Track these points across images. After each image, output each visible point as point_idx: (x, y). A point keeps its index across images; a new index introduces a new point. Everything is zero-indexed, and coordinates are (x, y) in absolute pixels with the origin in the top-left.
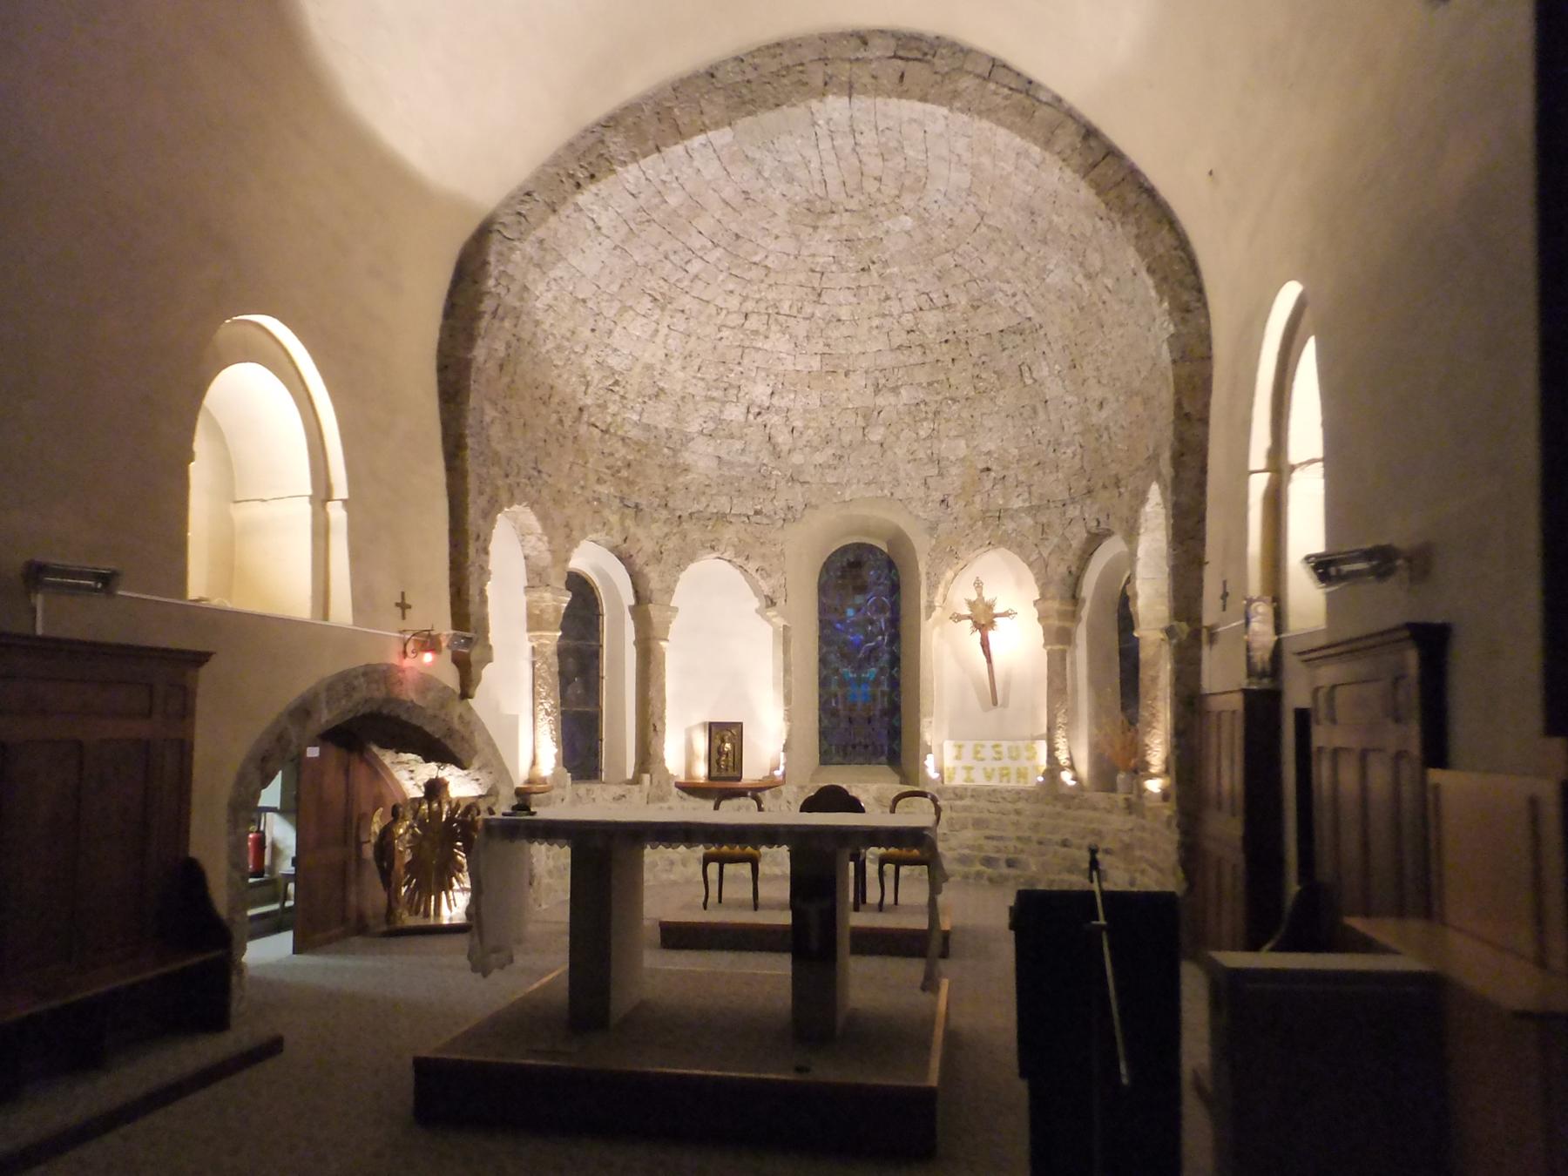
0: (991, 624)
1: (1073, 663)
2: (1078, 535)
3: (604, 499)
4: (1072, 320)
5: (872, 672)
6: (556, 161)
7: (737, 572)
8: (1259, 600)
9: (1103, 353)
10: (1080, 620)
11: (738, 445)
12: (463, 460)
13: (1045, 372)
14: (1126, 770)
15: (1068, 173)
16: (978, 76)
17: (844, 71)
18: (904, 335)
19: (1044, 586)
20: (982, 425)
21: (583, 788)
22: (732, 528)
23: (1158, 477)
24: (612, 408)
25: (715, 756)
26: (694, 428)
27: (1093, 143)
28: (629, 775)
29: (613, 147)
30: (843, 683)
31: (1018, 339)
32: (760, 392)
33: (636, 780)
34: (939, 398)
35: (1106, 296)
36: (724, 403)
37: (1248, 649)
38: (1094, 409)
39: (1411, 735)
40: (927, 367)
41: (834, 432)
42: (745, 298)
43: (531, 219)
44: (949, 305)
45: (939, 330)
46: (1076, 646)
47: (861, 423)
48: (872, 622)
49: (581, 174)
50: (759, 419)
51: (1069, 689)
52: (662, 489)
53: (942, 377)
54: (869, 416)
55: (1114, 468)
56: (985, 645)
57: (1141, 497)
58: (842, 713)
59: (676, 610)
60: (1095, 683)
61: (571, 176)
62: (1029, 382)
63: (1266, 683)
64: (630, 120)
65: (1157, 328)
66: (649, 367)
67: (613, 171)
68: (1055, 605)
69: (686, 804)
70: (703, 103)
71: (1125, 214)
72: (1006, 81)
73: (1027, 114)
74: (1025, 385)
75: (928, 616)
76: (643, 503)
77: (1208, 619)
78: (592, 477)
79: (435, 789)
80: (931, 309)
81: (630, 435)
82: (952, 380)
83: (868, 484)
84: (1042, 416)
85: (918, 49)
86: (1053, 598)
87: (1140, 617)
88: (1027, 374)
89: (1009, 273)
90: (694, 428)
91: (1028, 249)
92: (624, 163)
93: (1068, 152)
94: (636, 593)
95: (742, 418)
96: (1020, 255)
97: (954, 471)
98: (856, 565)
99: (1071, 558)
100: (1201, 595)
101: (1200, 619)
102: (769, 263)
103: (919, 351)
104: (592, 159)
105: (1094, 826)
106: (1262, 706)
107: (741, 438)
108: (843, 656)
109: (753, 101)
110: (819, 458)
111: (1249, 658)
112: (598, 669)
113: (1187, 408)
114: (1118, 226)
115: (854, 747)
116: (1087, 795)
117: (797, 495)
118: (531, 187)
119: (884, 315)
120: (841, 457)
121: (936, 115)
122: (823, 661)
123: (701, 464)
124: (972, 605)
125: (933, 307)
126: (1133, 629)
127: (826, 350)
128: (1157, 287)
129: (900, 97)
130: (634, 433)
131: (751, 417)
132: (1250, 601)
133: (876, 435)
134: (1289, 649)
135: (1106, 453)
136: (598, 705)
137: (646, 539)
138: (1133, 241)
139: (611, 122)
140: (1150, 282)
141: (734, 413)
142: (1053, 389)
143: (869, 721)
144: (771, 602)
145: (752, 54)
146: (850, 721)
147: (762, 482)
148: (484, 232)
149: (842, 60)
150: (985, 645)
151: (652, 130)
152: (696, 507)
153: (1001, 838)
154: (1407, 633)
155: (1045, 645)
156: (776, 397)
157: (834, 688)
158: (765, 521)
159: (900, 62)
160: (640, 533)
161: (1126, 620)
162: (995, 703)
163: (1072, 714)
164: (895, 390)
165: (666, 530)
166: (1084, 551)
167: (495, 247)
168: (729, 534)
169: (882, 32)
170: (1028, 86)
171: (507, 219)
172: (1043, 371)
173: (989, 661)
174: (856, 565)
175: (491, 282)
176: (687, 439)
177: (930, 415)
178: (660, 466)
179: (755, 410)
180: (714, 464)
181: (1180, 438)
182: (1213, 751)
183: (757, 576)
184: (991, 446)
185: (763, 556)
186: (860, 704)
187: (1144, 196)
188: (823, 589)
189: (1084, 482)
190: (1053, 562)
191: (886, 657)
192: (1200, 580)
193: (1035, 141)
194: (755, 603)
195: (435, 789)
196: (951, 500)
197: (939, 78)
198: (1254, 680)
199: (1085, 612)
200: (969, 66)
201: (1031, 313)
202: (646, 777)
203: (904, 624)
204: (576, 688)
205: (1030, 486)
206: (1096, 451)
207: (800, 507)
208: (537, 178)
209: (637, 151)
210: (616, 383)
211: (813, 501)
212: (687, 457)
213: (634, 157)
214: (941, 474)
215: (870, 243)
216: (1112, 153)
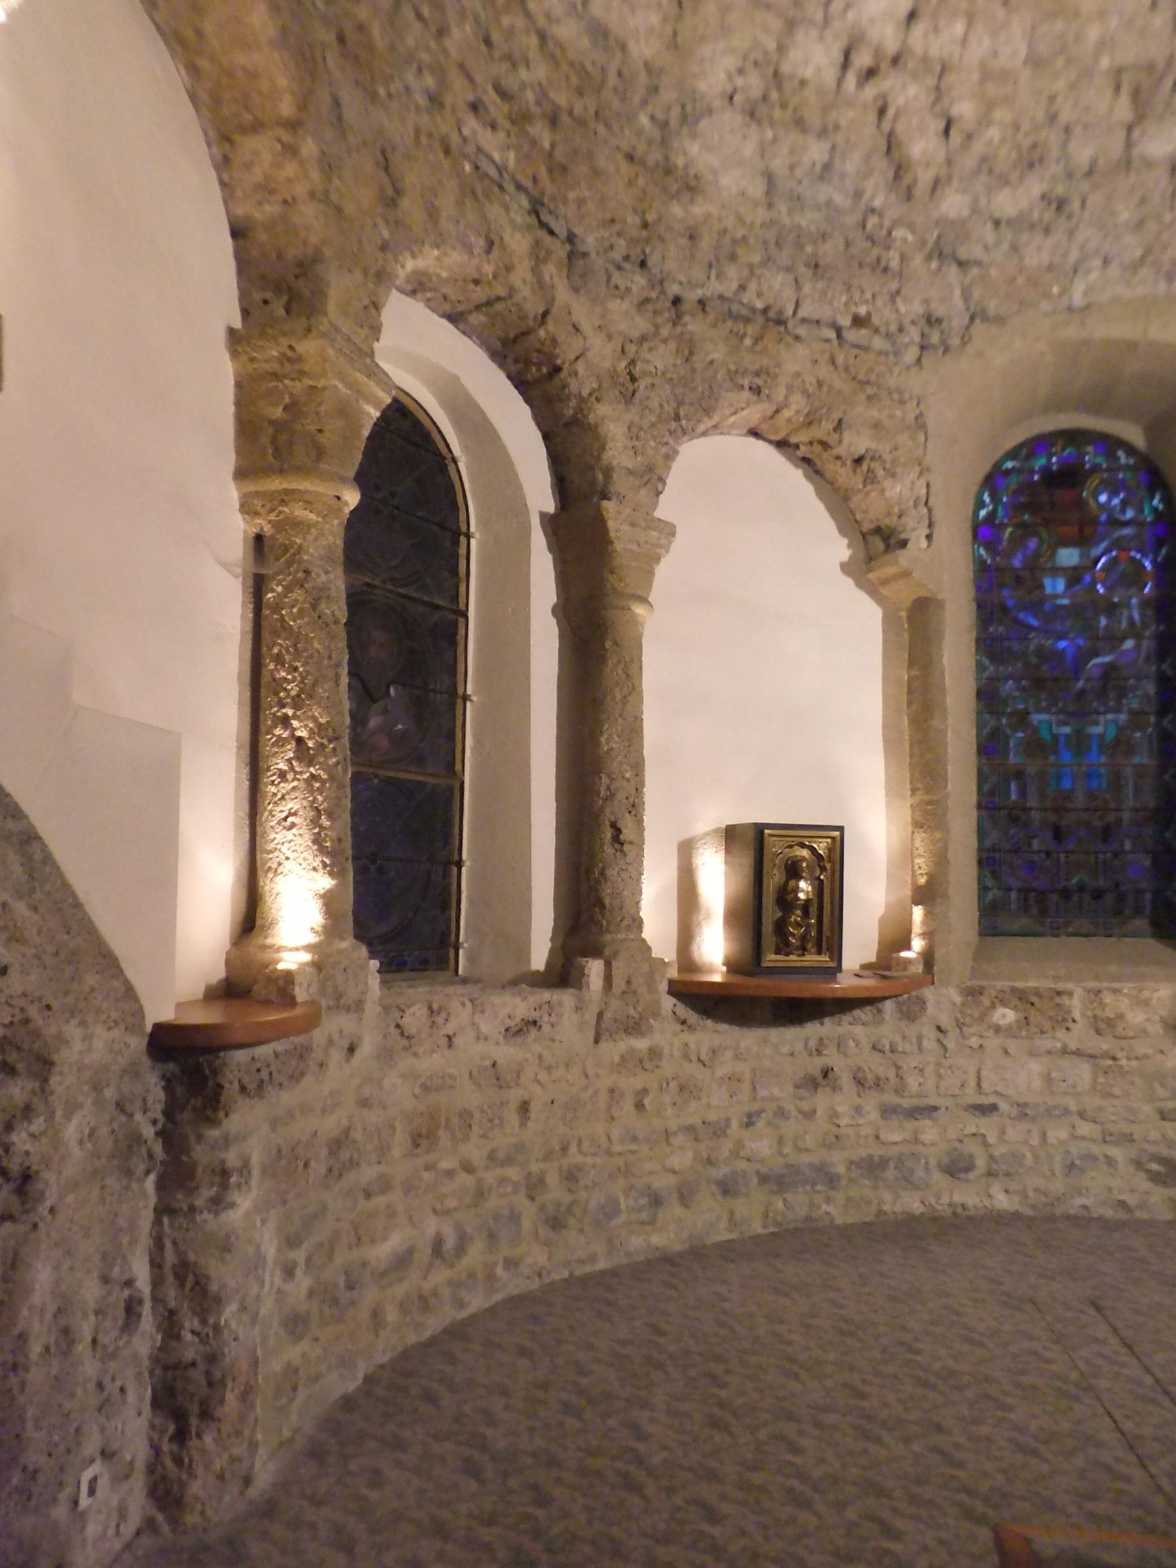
5: (1103, 726)
11: (816, 151)
21: (417, 996)
22: (801, 350)
25: (771, 913)
28: (539, 957)
33: (562, 974)
41: (1053, 139)
47: (1124, 110)
50: (870, 91)
52: (632, 220)
59: (669, 530)
69: (692, 1039)
76: (590, 241)
94: (561, 485)
95: (830, 75)
98: (1069, 477)
107: (823, 133)
110: (1007, 203)
112: (452, 669)
117: (946, 293)
120: (1061, 205)
123: (725, 181)
131: (851, 80)
136: (451, 767)
137: (595, 334)
141: (813, 58)
143: (1106, 833)
146: (1058, 834)
147: (871, 253)
152: (714, 287)
156: (919, 29)
157: (1014, 759)
158: (878, 343)
165: (642, 324)
174: (1069, 477)
176: (691, 114)
179: (863, 59)
194: (841, 549)
195: (1088, 453)
202: (595, 968)
204: (392, 715)
207: (959, 322)
211: (992, 307)
212: (694, 152)
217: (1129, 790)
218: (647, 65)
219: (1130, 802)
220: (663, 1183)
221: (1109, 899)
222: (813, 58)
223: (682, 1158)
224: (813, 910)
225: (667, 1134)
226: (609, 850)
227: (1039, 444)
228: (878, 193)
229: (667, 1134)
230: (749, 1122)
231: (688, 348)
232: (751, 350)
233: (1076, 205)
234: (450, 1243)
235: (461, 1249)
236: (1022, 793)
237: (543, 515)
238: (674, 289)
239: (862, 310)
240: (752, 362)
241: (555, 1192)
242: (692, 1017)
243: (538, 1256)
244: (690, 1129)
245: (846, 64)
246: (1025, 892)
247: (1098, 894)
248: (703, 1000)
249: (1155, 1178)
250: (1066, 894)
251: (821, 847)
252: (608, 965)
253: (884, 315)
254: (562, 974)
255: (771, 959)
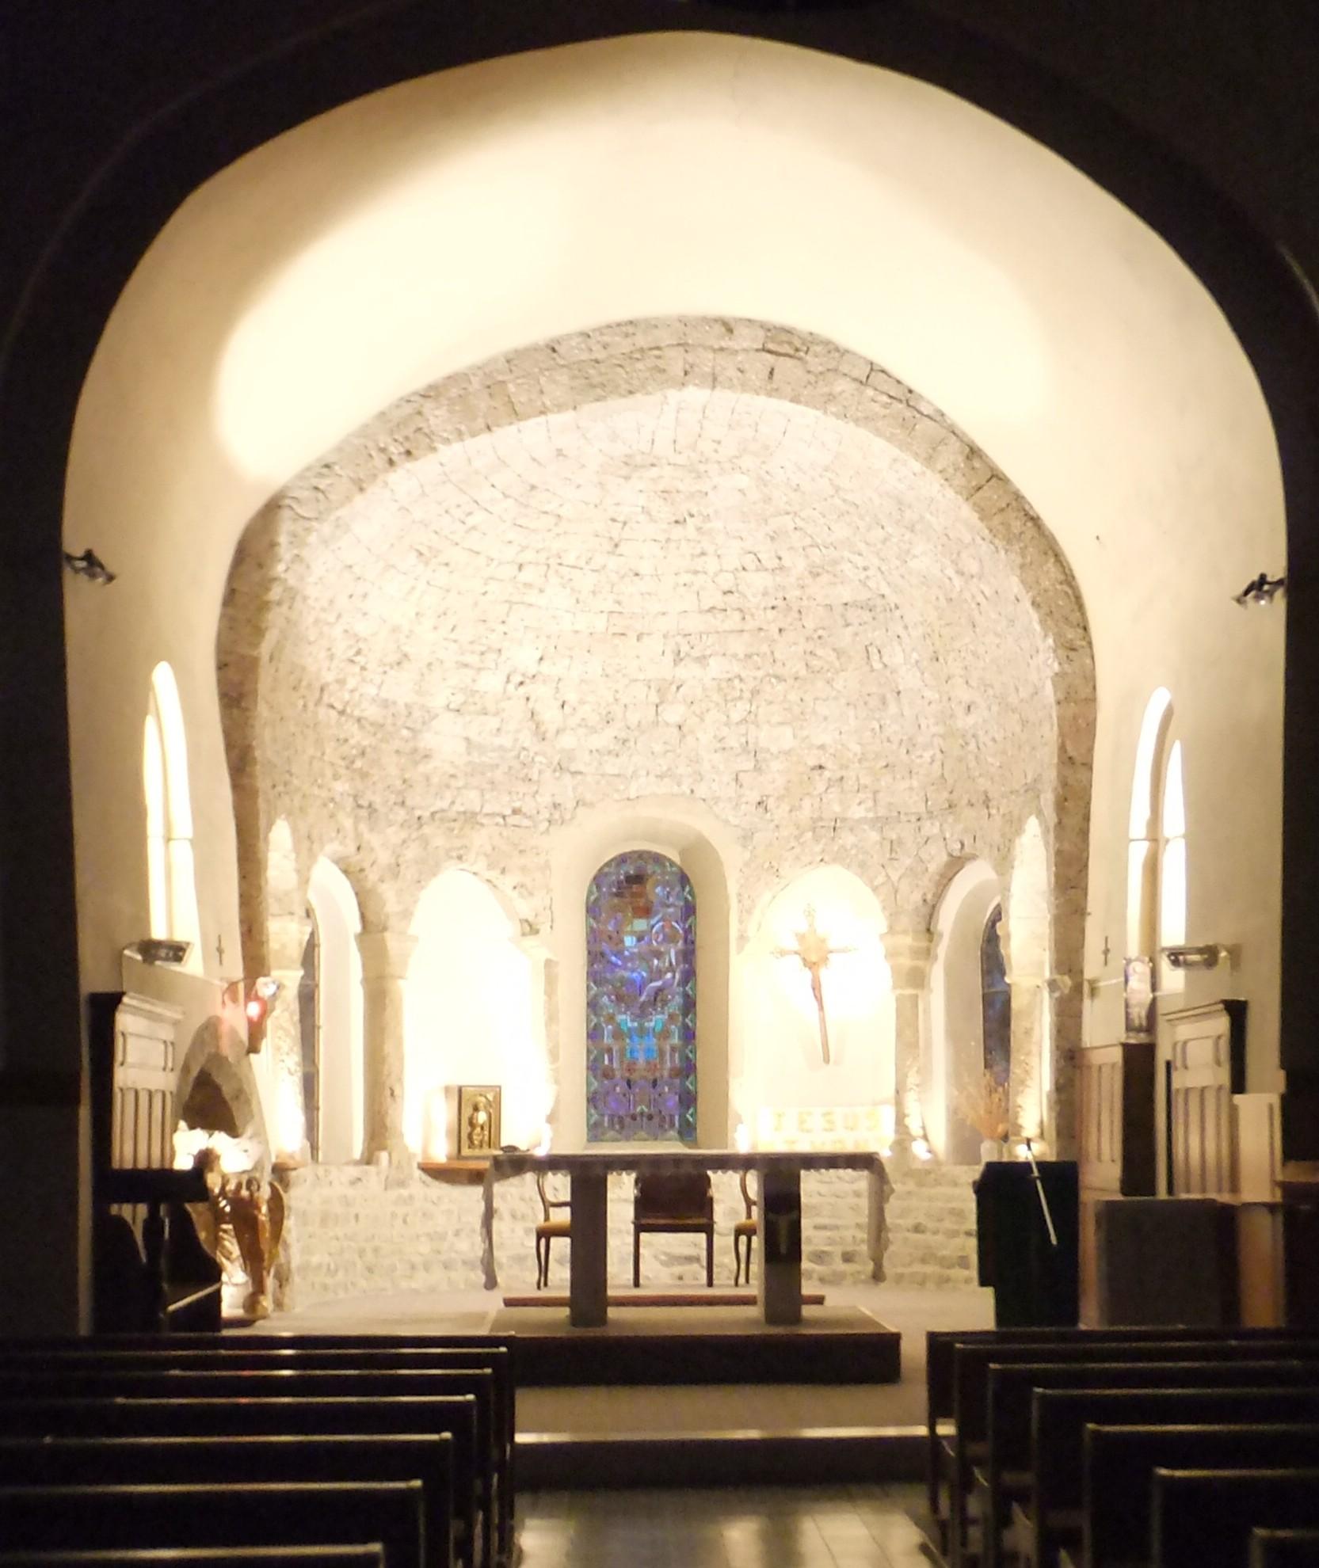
0: (825, 960)
1: (927, 1011)
2: (937, 859)
3: (338, 798)
4: (936, 608)
5: (656, 1021)
6: (364, 431)
7: (486, 887)
8: (1137, 960)
9: (974, 653)
10: (936, 958)
11: (493, 723)
12: (251, 776)
13: (899, 659)
14: (992, 1138)
15: (950, 493)
16: (855, 380)
17: (706, 361)
18: (719, 596)
19: (893, 916)
20: (814, 712)
23: (1039, 813)
24: (351, 683)
25: (466, 1129)
26: (438, 702)
27: (977, 464)
28: (358, 1149)
29: (432, 421)
30: (618, 1034)
31: (866, 616)
32: (524, 658)
33: (368, 1159)
34: (760, 674)
35: (980, 598)
36: (479, 669)
37: (1127, 1006)
38: (960, 711)
39: (1224, 1077)
40: (746, 636)
42: (524, 549)
43: (332, 497)
44: (781, 568)
45: (765, 594)
46: (931, 991)
48: (659, 955)
49: (395, 450)
50: (522, 690)
51: (921, 1043)
52: (398, 783)
53: (765, 648)
54: (664, 691)
55: (983, 783)
56: (816, 988)
57: (1015, 825)
58: (618, 1074)
60: (954, 1036)
61: (383, 450)
62: (877, 666)
63: (1142, 1038)
64: (454, 392)
65: (1041, 665)
66: (395, 630)
67: (434, 449)
68: (907, 941)
70: (543, 380)
71: (1009, 542)
72: (885, 388)
73: (907, 426)
74: (872, 670)
75: (740, 949)
76: (377, 800)
77: (1089, 972)
78: (329, 773)
79: (205, 1160)
80: (758, 570)
81: (366, 714)
82: (777, 655)
83: (660, 777)
84: (893, 708)
85: (790, 343)
86: (905, 932)
87: (1013, 962)
88: (875, 657)
89: (862, 547)
90: (438, 702)
91: (889, 529)
92: (447, 441)
93: (951, 470)
96: (879, 534)
97: (775, 765)
98: (638, 879)
99: (927, 885)
100: (1083, 946)
101: (1082, 972)
102: (561, 512)
103: (737, 616)
104: (409, 432)
105: (953, 1205)
106: (1140, 1063)
107: (497, 714)
108: (620, 999)
109: (603, 385)
111: (1127, 1014)
113: (1071, 752)
114: (1002, 552)
115: (634, 1118)
116: (944, 1169)
117: (565, 789)
118: (329, 460)
119: (696, 572)
120: (625, 741)
121: (805, 416)
122: (593, 1005)
124: (801, 938)
125: (760, 566)
126: (1003, 973)
127: (617, 608)
128: (1042, 622)
129: (769, 395)
130: (372, 712)
131: (511, 687)
132: (1129, 962)
133: (673, 714)
134: (1162, 1008)
135: (973, 764)
137: (382, 843)
138: (1018, 572)
139: (431, 393)
140: (1035, 616)
141: (491, 683)
142: (909, 679)
143: (655, 1083)
144: (530, 928)
145: (600, 330)
148: (272, 508)
149: (705, 348)
150: (816, 988)
151: (483, 406)
153: (837, 1227)
154: (1221, 1006)
155: (895, 987)
156: (545, 664)
157: (607, 1040)
158: (526, 822)
159: (769, 356)
160: (373, 839)
161: (992, 962)
162: (827, 1060)
163: (925, 1072)
164: (702, 660)
165: (403, 834)
166: (942, 876)
167: (285, 529)
168: (480, 839)
169: (750, 321)
170: (908, 397)
171: (304, 494)
172: (895, 656)
173: (821, 1008)
174: (638, 879)
175: (280, 568)
176: (430, 716)
177: (747, 695)
178: (397, 752)
179: (517, 679)
180: (461, 747)
181: (1064, 783)
182: (1094, 1105)
183: (515, 894)
184: (825, 738)
185: (524, 869)
186: (641, 1061)
187: (1029, 524)
188: (592, 910)
189: (945, 795)
190: (904, 886)
191: (678, 1000)
192: (1083, 931)
193: (916, 455)
195: (205, 1160)
196: (771, 803)
197: (812, 378)
198: (1131, 1034)
199: (942, 949)
200: (845, 368)
201: (885, 590)
203: (703, 962)
205: (875, 793)
206: (960, 759)
207: (571, 805)
208: (339, 449)
209: (463, 428)
210: (358, 653)
211: (589, 797)
212: (427, 740)
213: (460, 435)
214: (757, 769)
215: (691, 496)
216: (996, 476)
217: (668, 1057)
218: (406, 705)
219: (668, 1065)
220: (417, 1259)
221: (656, 1120)
222: (491, 683)
223: (425, 1248)
224: (486, 1128)
225: (418, 1237)
226: (389, 1099)
227: (622, 859)
228: (527, 739)
229: (418, 1237)
230: (457, 1234)
231: (425, 842)
232: (457, 837)
233: (632, 743)
234: (332, 1267)
235: (336, 1271)
236: (611, 1060)
237: (501, 1219)
238: (418, 813)
239: (517, 804)
240: (457, 843)
241: (370, 1256)
242: (428, 1179)
243: (363, 1283)
244: (428, 1235)
245: (508, 681)
246: (611, 1117)
247: (650, 1117)
248: (437, 1173)
249: (663, 1263)
250: (634, 1118)
251: (490, 1097)
252: (390, 1155)
253: (528, 806)
254: (368, 1159)
255: (466, 1151)
